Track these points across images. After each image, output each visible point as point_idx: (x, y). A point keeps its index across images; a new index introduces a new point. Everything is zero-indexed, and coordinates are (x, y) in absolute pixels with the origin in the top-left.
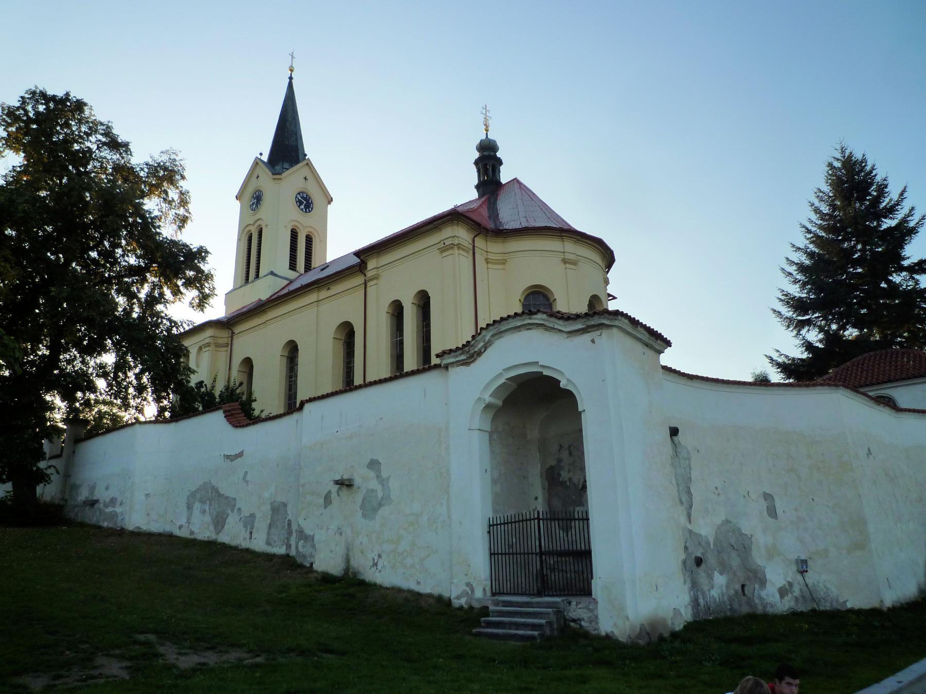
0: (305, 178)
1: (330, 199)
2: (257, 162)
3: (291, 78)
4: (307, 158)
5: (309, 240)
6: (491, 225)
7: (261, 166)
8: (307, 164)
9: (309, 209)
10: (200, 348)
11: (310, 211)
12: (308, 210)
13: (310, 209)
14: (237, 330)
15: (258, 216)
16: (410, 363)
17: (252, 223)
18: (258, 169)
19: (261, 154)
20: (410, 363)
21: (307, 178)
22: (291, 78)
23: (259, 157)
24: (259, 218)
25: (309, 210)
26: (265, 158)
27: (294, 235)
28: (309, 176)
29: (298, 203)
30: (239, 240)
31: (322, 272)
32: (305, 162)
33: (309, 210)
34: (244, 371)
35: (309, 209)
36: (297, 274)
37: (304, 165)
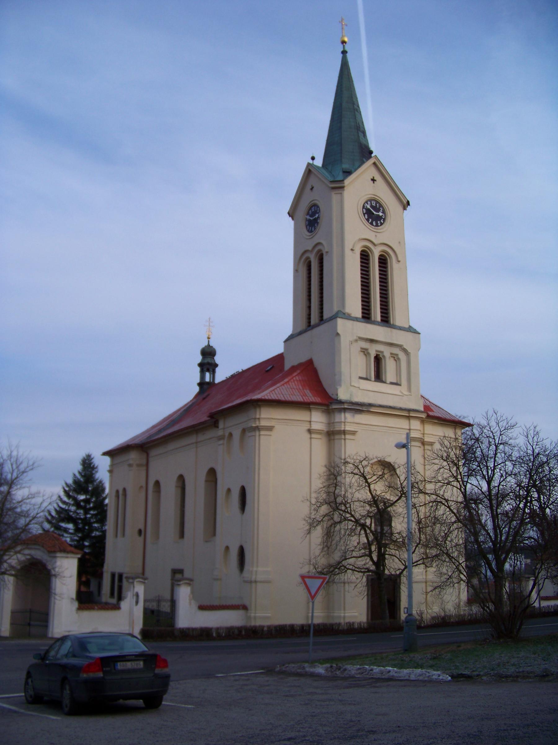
0: (373, 180)
1: (405, 202)
2: (310, 171)
3: (344, 52)
4: (373, 155)
5: (383, 261)
6: (39, 505)
7: (315, 174)
8: (374, 164)
9: (380, 221)
10: (244, 431)
11: (382, 224)
12: (379, 222)
13: (382, 221)
14: (153, 453)
15: (316, 240)
16: (314, 319)
17: (310, 249)
18: (312, 181)
19: (313, 158)
20: (314, 319)
21: (375, 179)
22: (344, 52)
23: (311, 162)
24: (317, 242)
25: (381, 223)
26: (319, 162)
27: (365, 257)
28: (378, 177)
29: (366, 216)
30: (296, 271)
31: (246, 567)
32: (371, 161)
33: (381, 223)
34: (320, 421)
35: (380, 221)
36: (313, 490)
37: (370, 166)
